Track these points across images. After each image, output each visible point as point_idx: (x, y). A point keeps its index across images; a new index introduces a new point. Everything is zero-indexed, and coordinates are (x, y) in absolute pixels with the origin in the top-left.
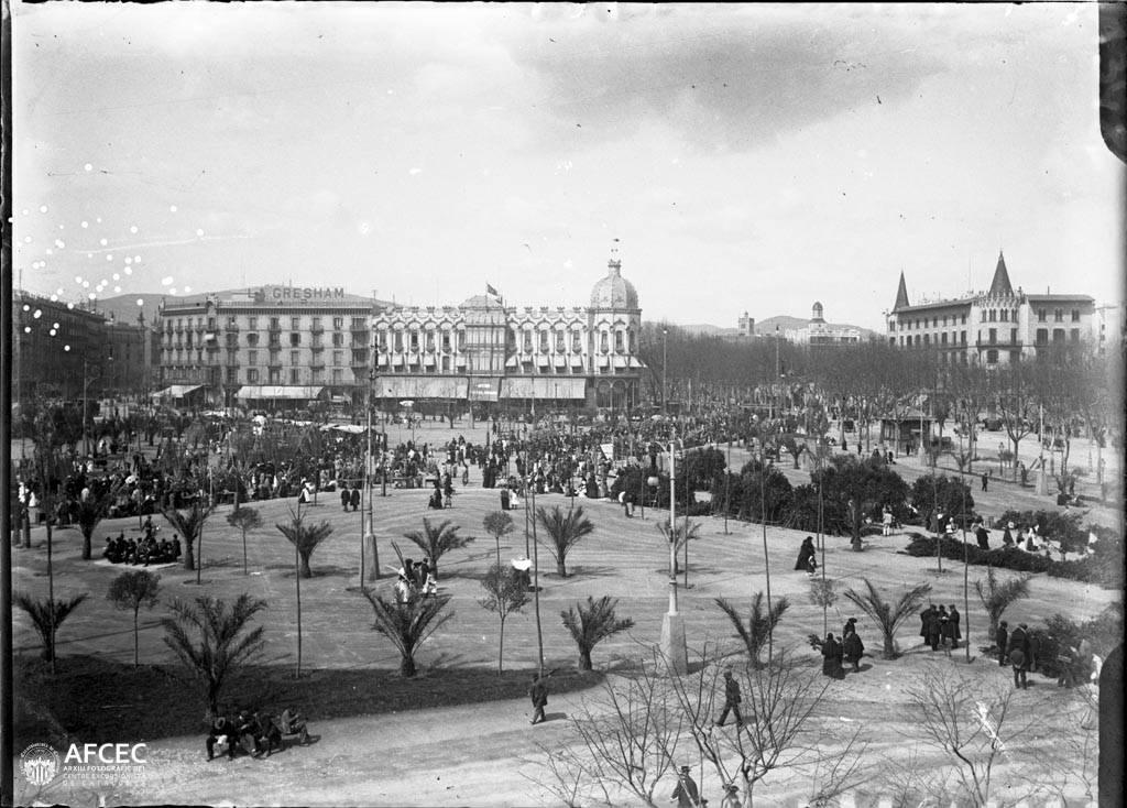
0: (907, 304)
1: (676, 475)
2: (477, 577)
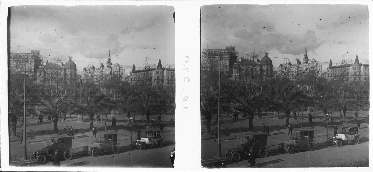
0: (135, 70)
1: (24, 106)
2: (172, 108)
